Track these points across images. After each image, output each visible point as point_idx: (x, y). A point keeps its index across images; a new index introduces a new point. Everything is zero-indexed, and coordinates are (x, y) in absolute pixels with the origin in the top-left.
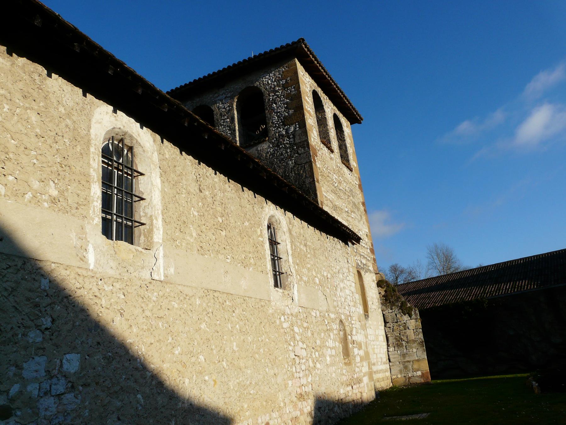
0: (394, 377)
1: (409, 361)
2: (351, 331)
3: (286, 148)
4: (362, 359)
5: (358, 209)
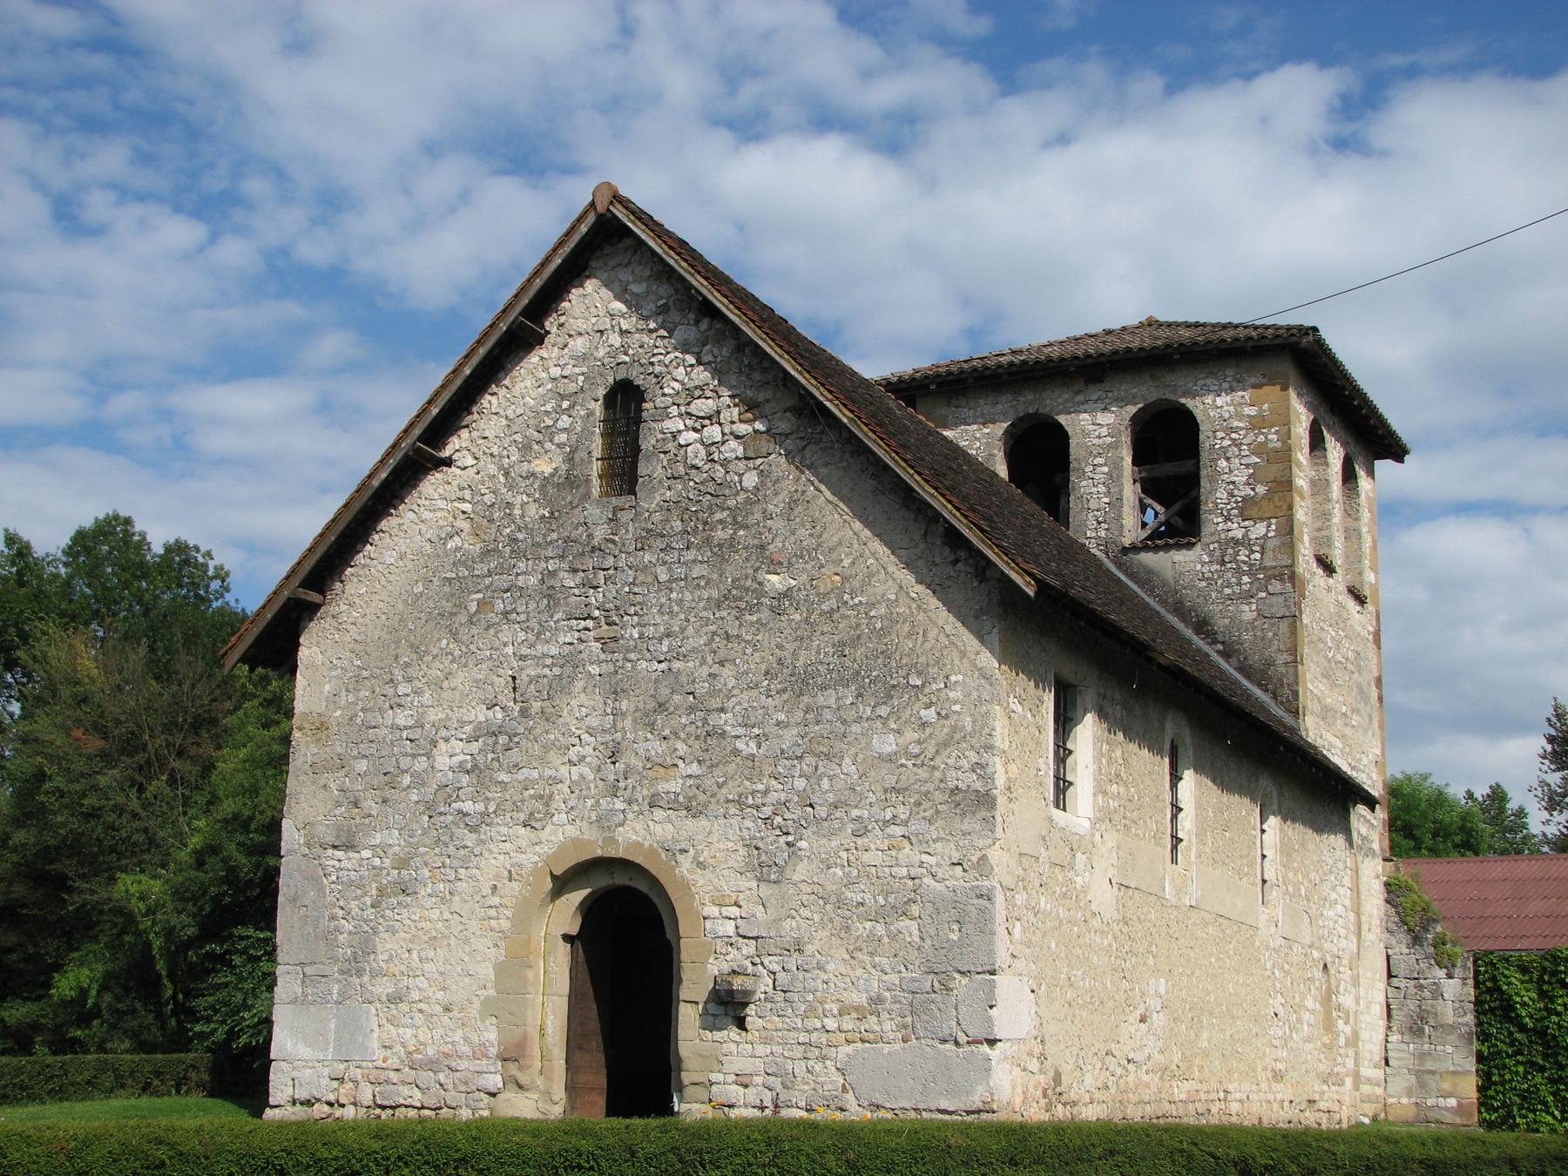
0: (1390, 1101)
1: (1432, 1072)
2: (1338, 987)
3: (1239, 572)
4: (1347, 1044)
5: (1366, 699)
